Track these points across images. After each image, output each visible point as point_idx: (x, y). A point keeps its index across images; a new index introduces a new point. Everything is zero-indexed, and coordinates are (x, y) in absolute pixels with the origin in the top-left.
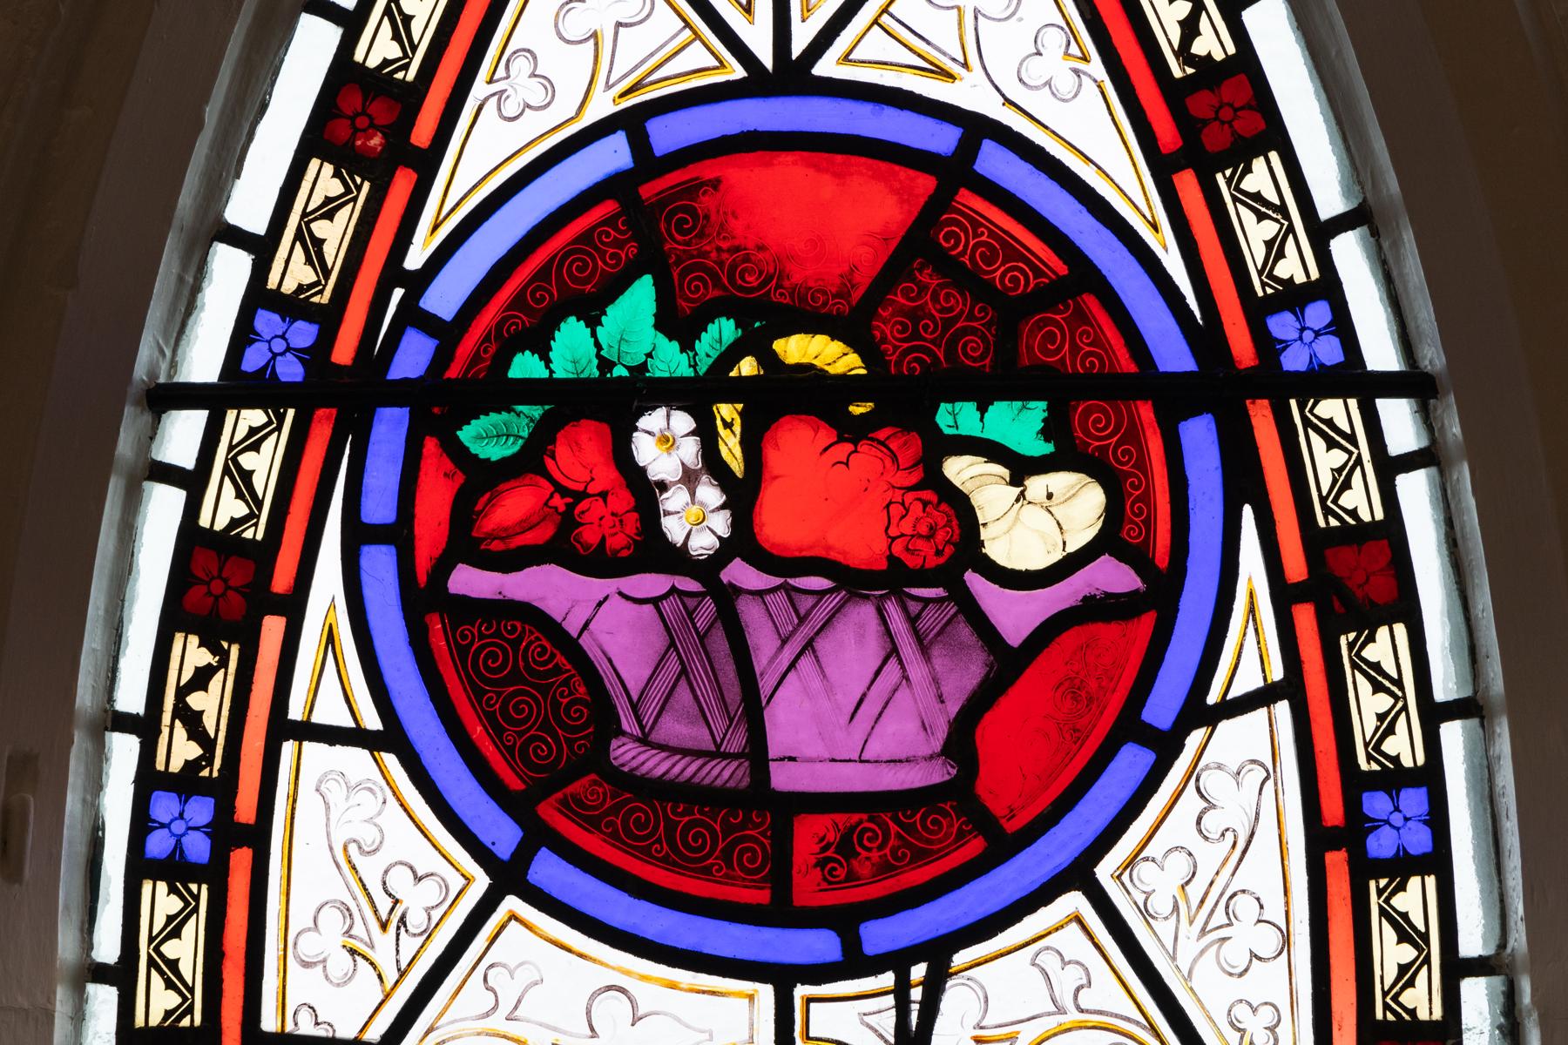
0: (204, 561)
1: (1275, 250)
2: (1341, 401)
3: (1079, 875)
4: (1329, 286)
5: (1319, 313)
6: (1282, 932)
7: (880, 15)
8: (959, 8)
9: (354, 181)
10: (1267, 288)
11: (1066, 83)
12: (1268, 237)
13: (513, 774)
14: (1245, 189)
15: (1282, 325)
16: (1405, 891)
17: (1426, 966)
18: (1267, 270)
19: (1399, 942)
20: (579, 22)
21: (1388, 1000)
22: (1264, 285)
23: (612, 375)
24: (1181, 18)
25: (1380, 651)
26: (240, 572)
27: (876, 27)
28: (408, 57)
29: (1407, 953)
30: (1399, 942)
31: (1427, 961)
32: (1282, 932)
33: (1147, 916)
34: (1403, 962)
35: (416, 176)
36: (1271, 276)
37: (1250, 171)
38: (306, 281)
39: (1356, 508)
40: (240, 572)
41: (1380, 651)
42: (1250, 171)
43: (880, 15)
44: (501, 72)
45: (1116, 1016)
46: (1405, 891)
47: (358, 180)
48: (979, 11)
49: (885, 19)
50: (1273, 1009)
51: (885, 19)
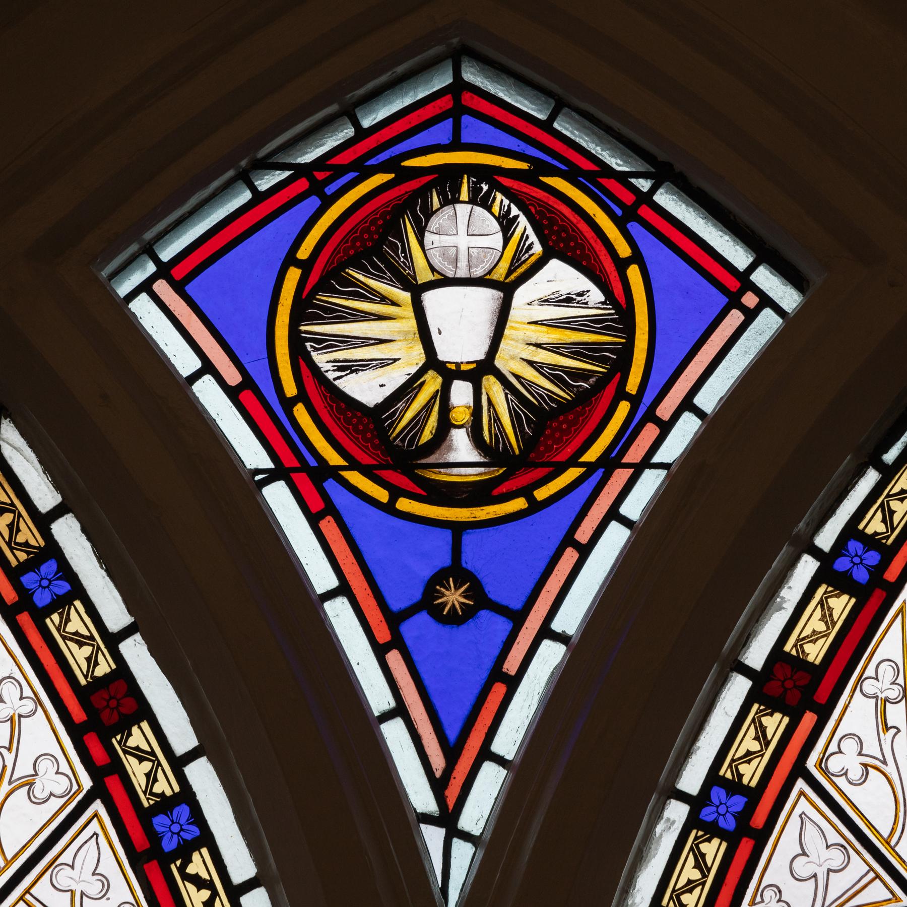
0: (129, 706)
1: (151, 777)
4: (187, 795)
5: (183, 812)
6: (833, 775)
7: (24, 895)
8: (71, 891)
10: (150, 801)
12: (147, 771)
14: (90, 647)
15: (160, 822)
16: (710, 843)
18: (148, 791)
20: (803, 867)
22: (148, 799)
24: (79, 631)
25: (75, 625)
27: (21, 902)
32: (833, 775)
34: (87, 656)
36: (152, 794)
37: (131, 735)
39: (163, 791)
41: (75, 625)
42: (131, 735)
43: (24, 895)
45: (904, 825)
46: (710, 843)
48: (84, 893)
49: (28, 897)
51: (28, 897)
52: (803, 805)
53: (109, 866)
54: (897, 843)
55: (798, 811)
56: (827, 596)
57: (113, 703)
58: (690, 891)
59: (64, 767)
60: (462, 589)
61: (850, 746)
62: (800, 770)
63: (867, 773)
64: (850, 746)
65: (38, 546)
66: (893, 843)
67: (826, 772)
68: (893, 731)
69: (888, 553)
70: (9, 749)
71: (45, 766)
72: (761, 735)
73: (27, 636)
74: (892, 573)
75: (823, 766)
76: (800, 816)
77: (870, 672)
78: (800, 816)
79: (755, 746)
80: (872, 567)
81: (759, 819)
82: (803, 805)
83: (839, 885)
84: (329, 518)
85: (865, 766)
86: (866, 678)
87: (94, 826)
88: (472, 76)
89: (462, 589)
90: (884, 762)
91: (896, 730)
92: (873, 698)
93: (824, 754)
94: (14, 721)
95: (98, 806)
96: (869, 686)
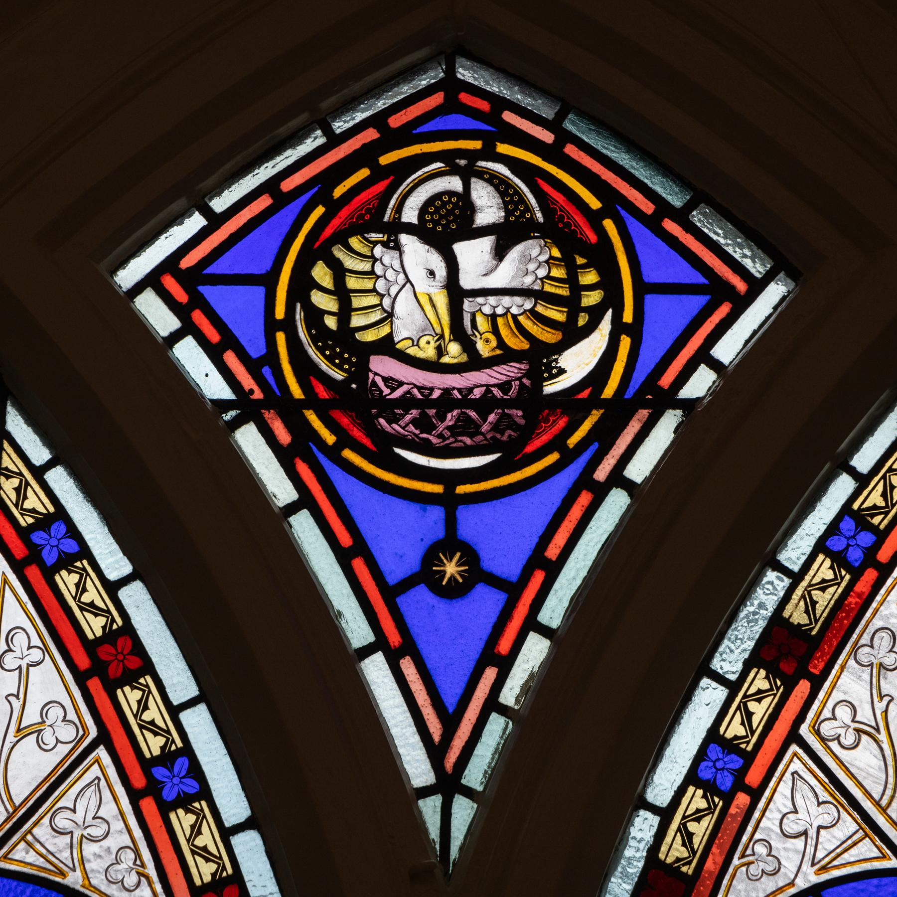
0: (134, 663)
2: (695, 788)
3: (867, 835)
9: (840, 572)
11: (131, 880)
13: (23, 799)
17: (748, 694)
19: (753, 713)
21: (775, 692)
23: (583, 266)
26: (114, 671)
28: (682, 824)
29: (752, 706)
30: (753, 713)
31: (745, 696)
33: (853, 653)
35: (263, 370)
38: (162, 744)
40: (114, 671)
44: (749, 852)
47: (779, 683)
50: (838, 706)
52: (796, 766)
53: (109, 810)
54: (889, 804)
55: (792, 768)
56: (170, 741)
57: (120, 657)
58: (77, 585)
59: (72, 716)
60: (445, 561)
61: (844, 713)
62: (794, 737)
63: (859, 740)
64: (844, 713)
65: (47, 512)
66: (884, 803)
67: (818, 733)
68: (887, 699)
69: (882, 536)
70: (17, 697)
71: (55, 713)
72: (204, 853)
73: (489, 571)
74: (884, 555)
75: (816, 728)
76: (793, 774)
77: (865, 639)
78: (793, 774)
79: (200, 842)
80: (66, 533)
81: (753, 777)
82: (796, 766)
83: (829, 841)
84: (37, 464)
85: (858, 731)
86: (862, 646)
87: (95, 771)
88: (465, 74)
89: (445, 561)
90: (878, 730)
91: (890, 698)
92: (868, 666)
93: (818, 718)
94: (23, 673)
95: (102, 752)
96: (864, 654)
